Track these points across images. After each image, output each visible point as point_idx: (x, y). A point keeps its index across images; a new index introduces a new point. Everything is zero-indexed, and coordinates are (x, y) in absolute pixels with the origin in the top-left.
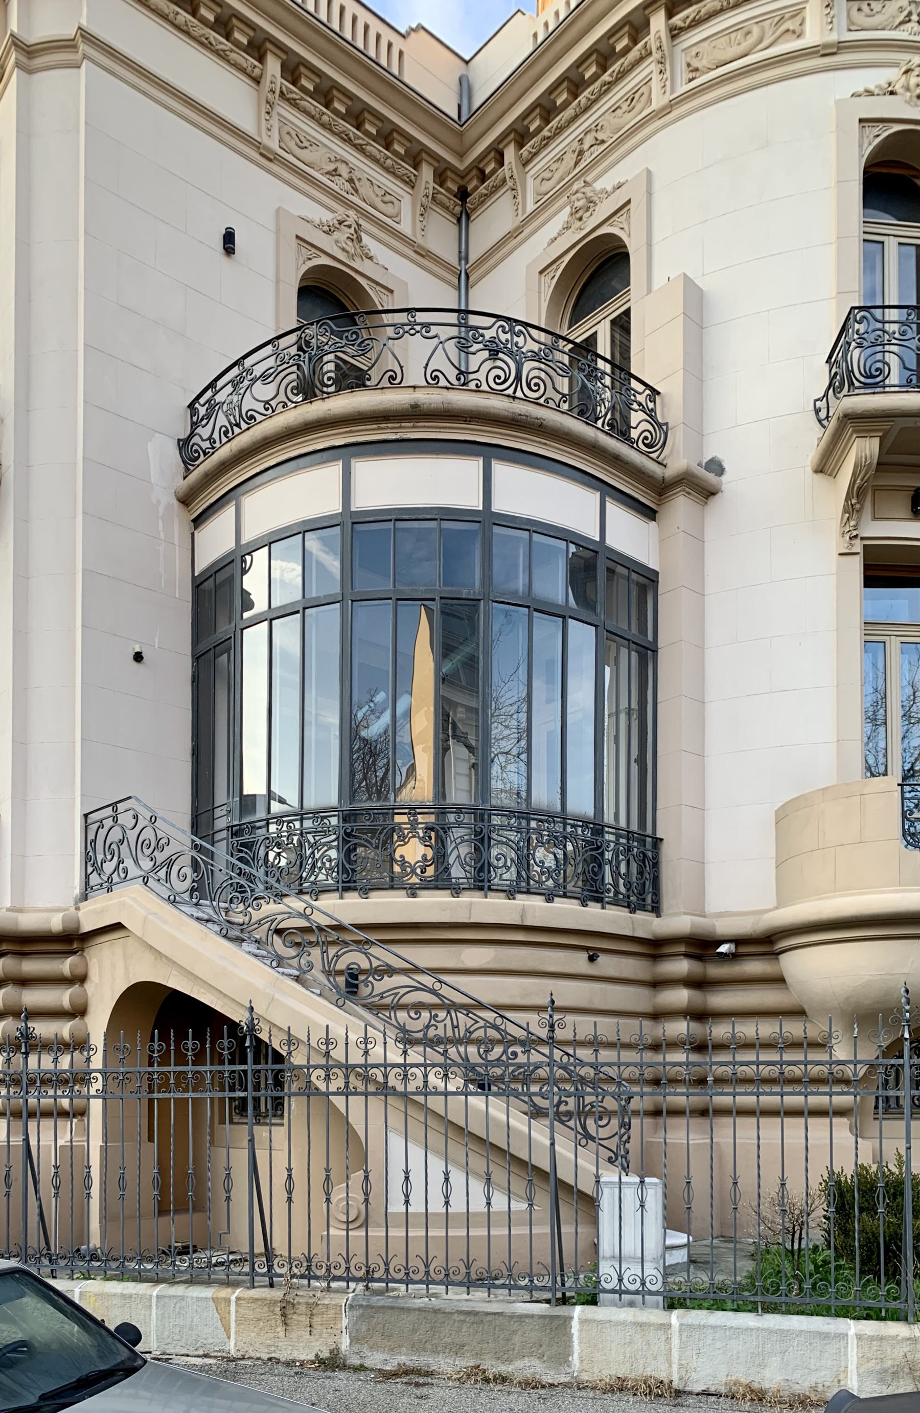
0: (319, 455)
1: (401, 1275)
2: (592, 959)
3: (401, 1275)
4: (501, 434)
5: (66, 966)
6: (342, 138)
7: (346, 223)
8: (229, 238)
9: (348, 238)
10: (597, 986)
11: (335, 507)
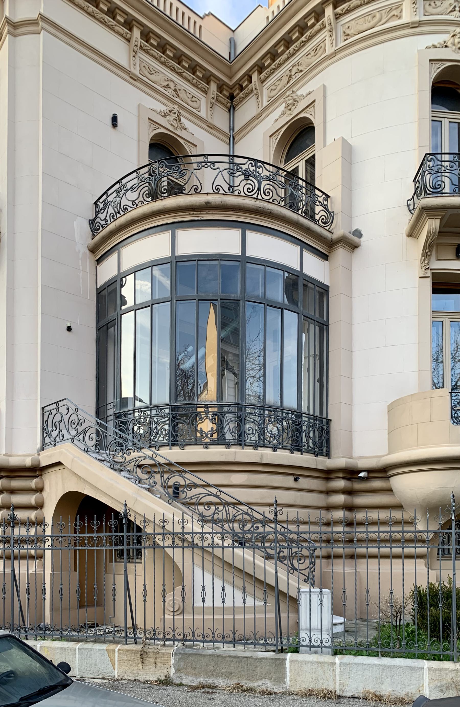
0: (160, 227)
1: (200, 638)
2: (296, 480)
3: (200, 638)
4: (250, 217)
5: (33, 483)
6: (171, 69)
7: (173, 112)
8: (114, 119)
9: (174, 119)
10: (299, 493)
11: (168, 253)
